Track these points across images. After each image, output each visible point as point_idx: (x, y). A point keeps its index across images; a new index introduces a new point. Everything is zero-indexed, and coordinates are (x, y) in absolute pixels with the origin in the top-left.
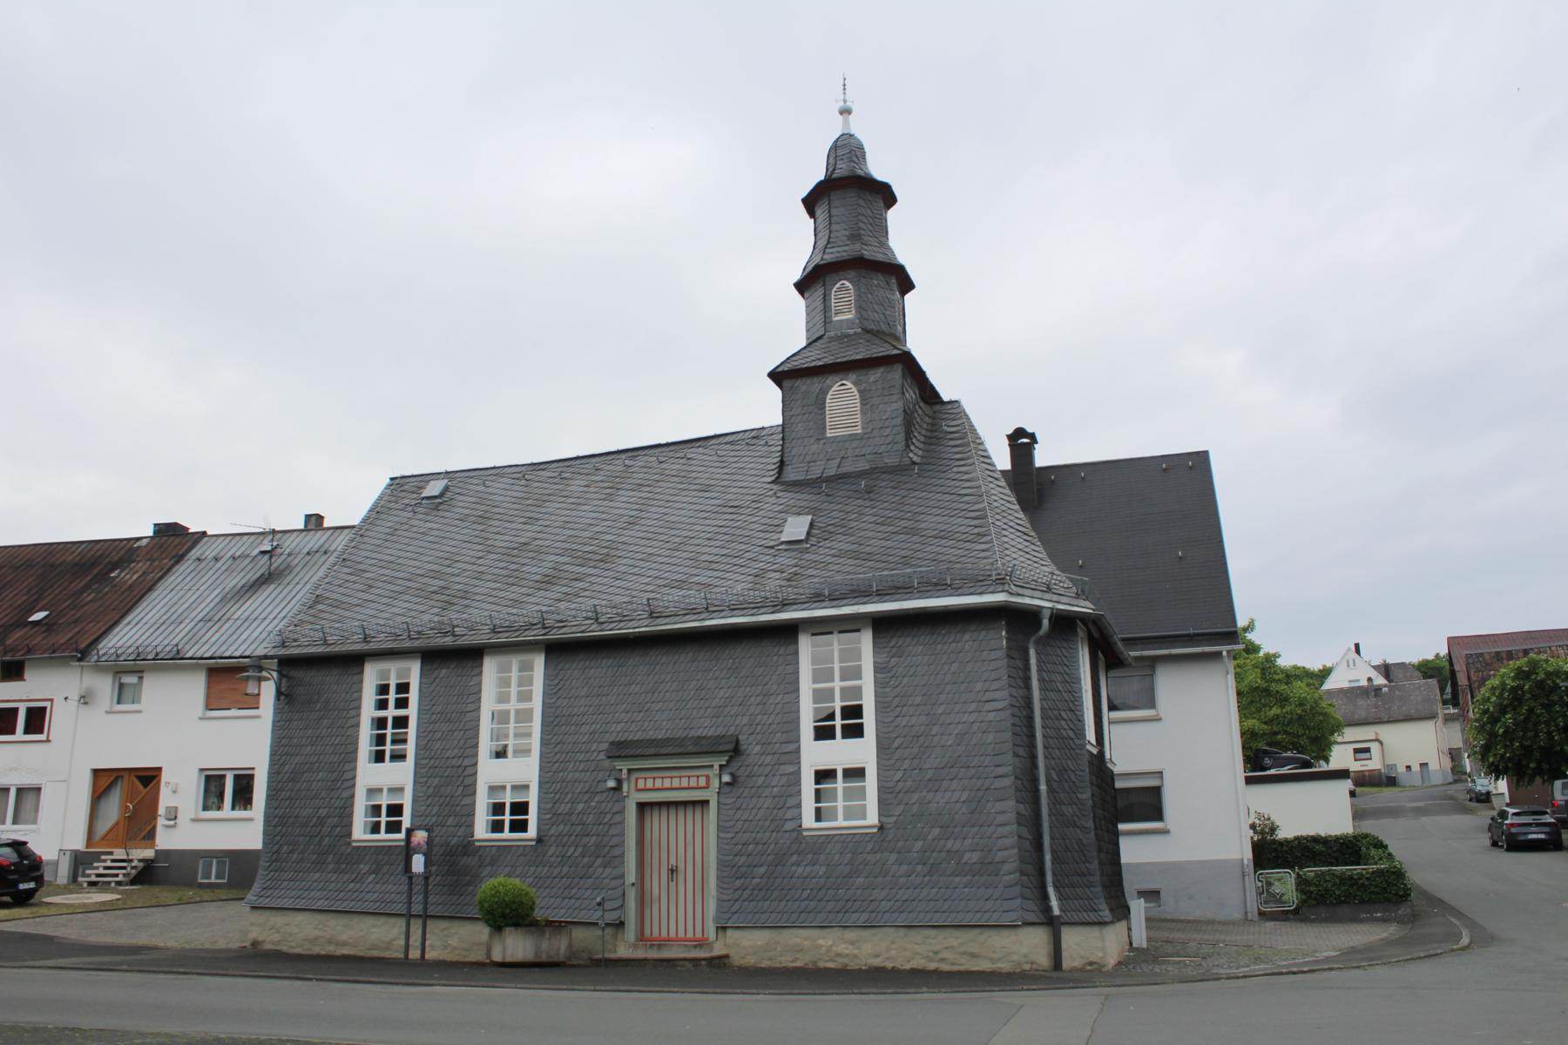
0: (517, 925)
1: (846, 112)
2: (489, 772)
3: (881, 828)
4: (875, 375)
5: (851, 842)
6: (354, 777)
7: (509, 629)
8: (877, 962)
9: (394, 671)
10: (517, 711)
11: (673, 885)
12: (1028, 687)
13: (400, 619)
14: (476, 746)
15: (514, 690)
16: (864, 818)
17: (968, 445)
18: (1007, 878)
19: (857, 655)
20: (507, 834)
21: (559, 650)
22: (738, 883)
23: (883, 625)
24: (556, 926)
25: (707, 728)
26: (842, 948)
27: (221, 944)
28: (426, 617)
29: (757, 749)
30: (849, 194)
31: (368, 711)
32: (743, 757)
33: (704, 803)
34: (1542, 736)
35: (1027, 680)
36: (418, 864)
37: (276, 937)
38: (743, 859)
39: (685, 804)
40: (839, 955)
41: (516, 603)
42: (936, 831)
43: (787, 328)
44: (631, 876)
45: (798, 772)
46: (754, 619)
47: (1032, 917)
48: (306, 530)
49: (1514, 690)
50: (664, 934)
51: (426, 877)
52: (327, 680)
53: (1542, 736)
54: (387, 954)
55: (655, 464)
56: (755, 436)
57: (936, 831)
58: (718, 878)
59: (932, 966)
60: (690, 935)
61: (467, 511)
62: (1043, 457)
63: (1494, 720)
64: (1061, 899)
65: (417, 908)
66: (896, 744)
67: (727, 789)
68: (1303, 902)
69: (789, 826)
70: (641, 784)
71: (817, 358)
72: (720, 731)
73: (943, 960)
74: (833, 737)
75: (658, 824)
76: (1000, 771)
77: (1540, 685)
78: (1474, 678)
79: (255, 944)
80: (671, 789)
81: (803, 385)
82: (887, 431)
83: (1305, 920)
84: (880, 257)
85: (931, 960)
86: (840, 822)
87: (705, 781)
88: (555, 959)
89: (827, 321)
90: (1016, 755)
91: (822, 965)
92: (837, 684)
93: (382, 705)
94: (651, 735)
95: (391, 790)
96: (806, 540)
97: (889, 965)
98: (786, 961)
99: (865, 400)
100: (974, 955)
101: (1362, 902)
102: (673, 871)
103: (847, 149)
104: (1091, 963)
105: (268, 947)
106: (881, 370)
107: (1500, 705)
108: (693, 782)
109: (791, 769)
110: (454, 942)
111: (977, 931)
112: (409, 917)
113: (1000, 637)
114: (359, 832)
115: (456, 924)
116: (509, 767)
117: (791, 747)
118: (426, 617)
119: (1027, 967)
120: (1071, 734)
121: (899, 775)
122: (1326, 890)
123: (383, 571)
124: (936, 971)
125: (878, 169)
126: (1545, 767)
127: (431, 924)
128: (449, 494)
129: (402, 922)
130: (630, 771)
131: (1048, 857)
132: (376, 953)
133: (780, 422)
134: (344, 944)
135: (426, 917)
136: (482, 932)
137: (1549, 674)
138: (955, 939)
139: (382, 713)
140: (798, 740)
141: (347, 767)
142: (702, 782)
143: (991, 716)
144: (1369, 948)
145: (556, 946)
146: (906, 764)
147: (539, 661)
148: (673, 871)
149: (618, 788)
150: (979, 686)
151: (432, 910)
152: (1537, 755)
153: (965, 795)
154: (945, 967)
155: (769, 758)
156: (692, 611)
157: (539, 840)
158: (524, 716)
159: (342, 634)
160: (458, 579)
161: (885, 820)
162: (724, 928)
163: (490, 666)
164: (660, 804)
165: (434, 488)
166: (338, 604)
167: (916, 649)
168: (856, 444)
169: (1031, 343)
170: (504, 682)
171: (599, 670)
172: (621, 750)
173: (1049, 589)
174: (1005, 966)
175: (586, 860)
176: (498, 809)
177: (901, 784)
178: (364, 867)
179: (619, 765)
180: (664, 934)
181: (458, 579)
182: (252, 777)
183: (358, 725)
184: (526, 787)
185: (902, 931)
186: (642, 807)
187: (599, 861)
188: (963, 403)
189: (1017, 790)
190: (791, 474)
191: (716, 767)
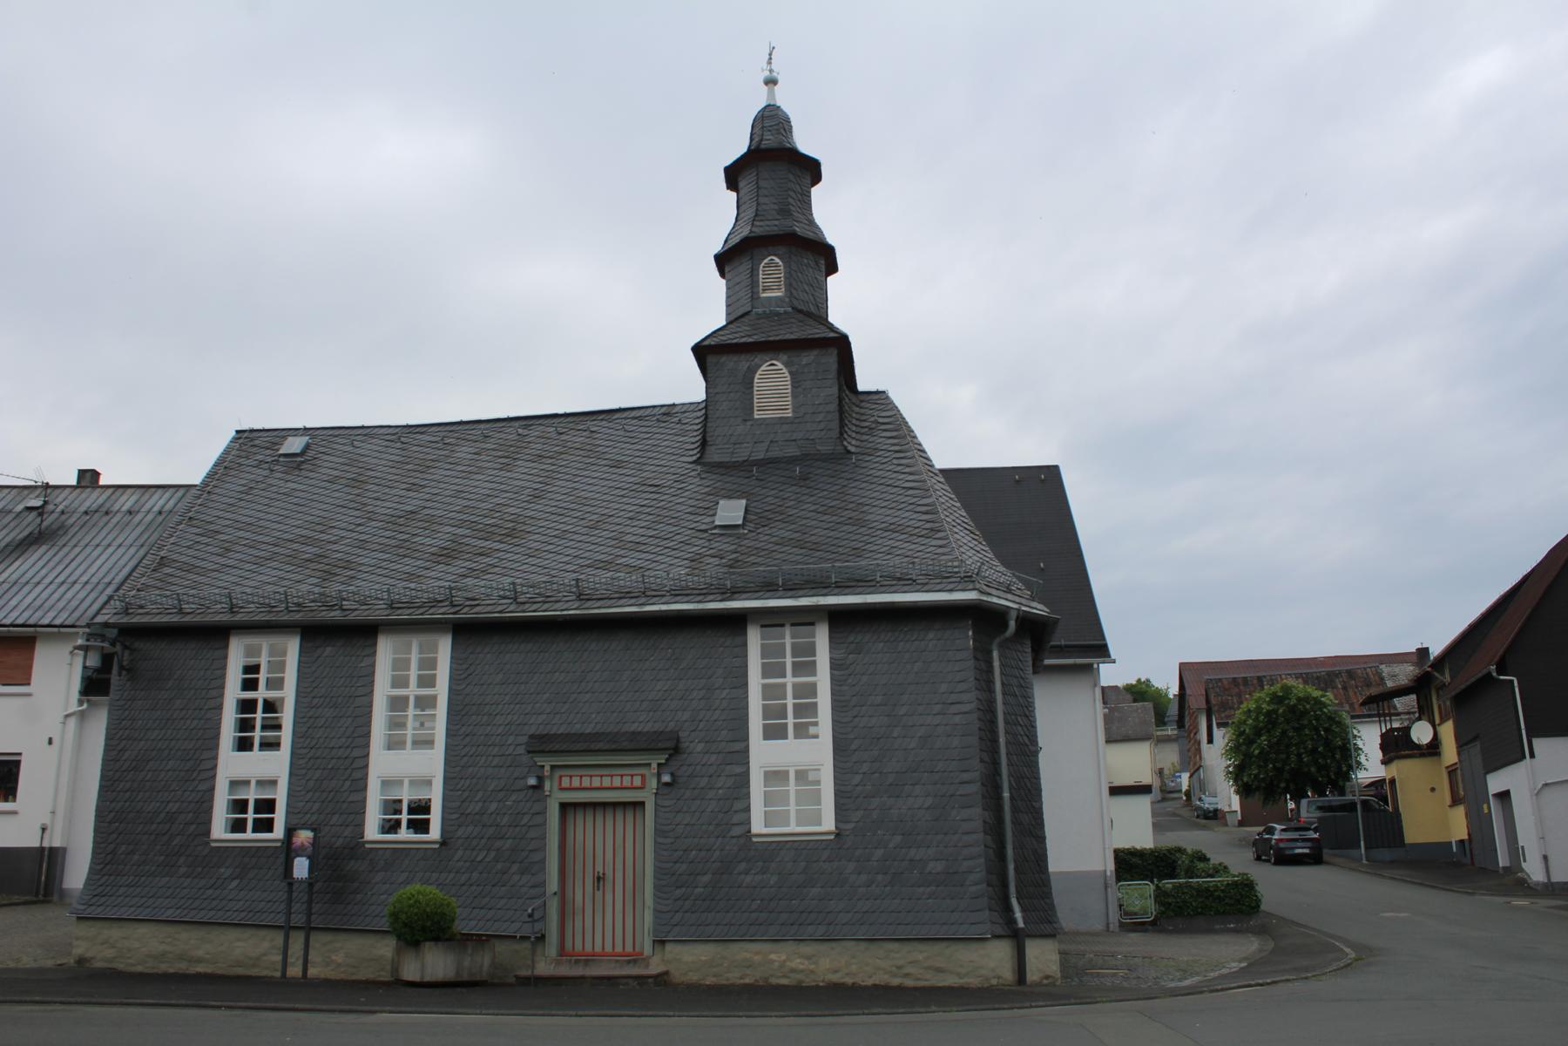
0: (436, 939)
1: (771, 82)
2: (232, 764)
3: (838, 834)
4: (808, 358)
5: (803, 849)
6: (215, 767)
7: (410, 605)
8: (835, 978)
9: (265, 647)
10: (418, 698)
11: (599, 894)
12: (991, 691)
13: (270, 588)
14: (368, 735)
15: (413, 674)
16: (427, 832)
17: (904, 437)
18: (973, 889)
19: (811, 650)
20: (404, 834)
21: (468, 631)
22: (678, 892)
23: (840, 619)
24: (481, 940)
25: (643, 723)
26: (797, 963)
27: (27, 962)
28: (304, 588)
29: (700, 747)
30: (773, 168)
31: (233, 691)
32: (697, 760)
33: (638, 805)
34: (1293, 758)
35: (990, 682)
36: (301, 868)
37: (110, 953)
38: (684, 866)
39: (615, 805)
40: (793, 971)
41: (411, 577)
42: (898, 838)
44: (553, 885)
45: (746, 776)
46: (664, 607)
47: (999, 931)
48: (79, 486)
49: (1269, 713)
50: (588, 948)
51: (310, 883)
52: (183, 656)
53: (1293, 758)
54: (254, 972)
55: (554, 435)
56: (667, 413)
57: (898, 838)
58: (656, 887)
59: (896, 982)
60: (619, 949)
61: (335, 473)
63: (1250, 742)
64: (1023, 910)
65: (298, 919)
66: (853, 747)
69: (736, 831)
70: (565, 782)
71: (741, 336)
72: (658, 727)
73: (907, 975)
74: (785, 737)
75: (585, 830)
76: (965, 776)
77: (1292, 709)
78: (1213, 701)
79: (81, 961)
80: (591, 789)
81: (729, 362)
82: (820, 417)
83: (1163, 931)
84: (811, 235)
85: (895, 976)
86: (793, 828)
87: (640, 781)
89: (754, 296)
90: (982, 761)
91: (774, 981)
92: (790, 680)
93: (250, 685)
94: (577, 728)
95: (260, 783)
96: (743, 526)
97: (849, 981)
98: (734, 977)
99: (795, 384)
100: (939, 970)
102: (599, 879)
103: (771, 122)
104: (1047, 977)
105: (99, 965)
106: (815, 352)
107: (1255, 727)
108: (627, 781)
109: (739, 770)
110: (339, 958)
111: (944, 944)
112: (288, 929)
113: (966, 638)
114: (219, 830)
115: (342, 937)
116: (407, 764)
117: (738, 746)
118: (304, 588)
119: (994, 982)
121: (857, 779)
123: (241, 534)
124: (900, 988)
125: (805, 142)
126: (1292, 786)
127: (318, 939)
128: (311, 453)
129: (279, 938)
130: (553, 767)
131: (1011, 867)
132: (240, 971)
133: (703, 397)
134: (199, 961)
135: (309, 929)
136: (386, 948)
137: (1299, 699)
138: (921, 953)
139: (249, 695)
140: (747, 739)
141: (205, 755)
142: (637, 782)
143: (957, 719)
145: (480, 963)
146: (865, 768)
147: (444, 647)
148: (599, 879)
149: (539, 787)
150: (944, 688)
151: (316, 921)
152: (1286, 775)
153: (929, 801)
154: (909, 983)
155: (714, 757)
156: (626, 595)
157: (444, 843)
158: (426, 703)
159: (203, 597)
160: (335, 547)
161: (842, 826)
162: (663, 942)
163: (385, 650)
164: (584, 806)
165: (294, 445)
166: (191, 568)
167: (497, 658)
168: (785, 427)
169: (948, 342)
170: (400, 665)
171: (516, 655)
172: (542, 744)
173: (1009, 591)
174: (973, 981)
175: (499, 866)
176: (240, 806)
177: (859, 788)
178: (225, 872)
179: (540, 761)
180: (588, 948)
181: (335, 547)
182: (18, 762)
183: (220, 707)
184: (274, 783)
185: (863, 945)
186: (564, 806)
187: (515, 867)
188: (895, 397)
189: (984, 797)
190: (714, 455)
191: (654, 765)
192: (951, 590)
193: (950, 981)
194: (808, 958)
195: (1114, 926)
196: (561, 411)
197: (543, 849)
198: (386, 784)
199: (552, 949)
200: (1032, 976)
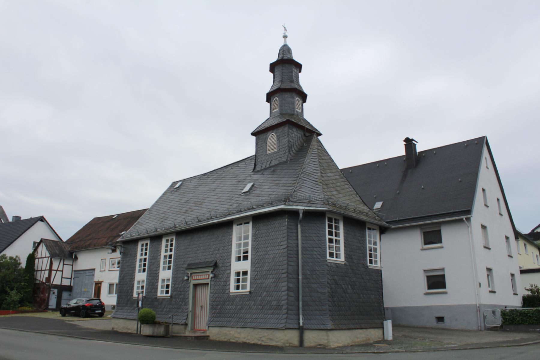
1: (285, 37)
4: (280, 130)
8: (244, 340)
26: (236, 335)
30: (285, 66)
32: (218, 268)
33: (208, 284)
40: (235, 337)
43: (262, 113)
44: (190, 309)
52: (130, 247)
59: (259, 343)
62: (419, 149)
67: (213, 279)
68: (503, 323)
73: (262, 341)
88: (159, 335)
94: (197, 261)
97: (248, 341)
98: (223, 339)
100: (271, 340)
101: (529, 324)
102: (202, 307)
103: (285, 49)
104: (320, 345)
113: (285, 221)
120: (319, 256)
122: (513, 318)
130: (191, 274)
131: (301, 303)
134: (129, 329)
144: (514, 341)
149: (188, 280)
154: (263, 343)
167: (264, 227)
172: (190, 267)
185: (252, 329)
190: (258, 169)
192: (297, 206)
193: (273, 343)
194: (239, 333)
195: (483, 329)
196: (235, 162)
197: (188, 298)
198: (139, 282)
199: (189, 327)
200: (306, 344)
